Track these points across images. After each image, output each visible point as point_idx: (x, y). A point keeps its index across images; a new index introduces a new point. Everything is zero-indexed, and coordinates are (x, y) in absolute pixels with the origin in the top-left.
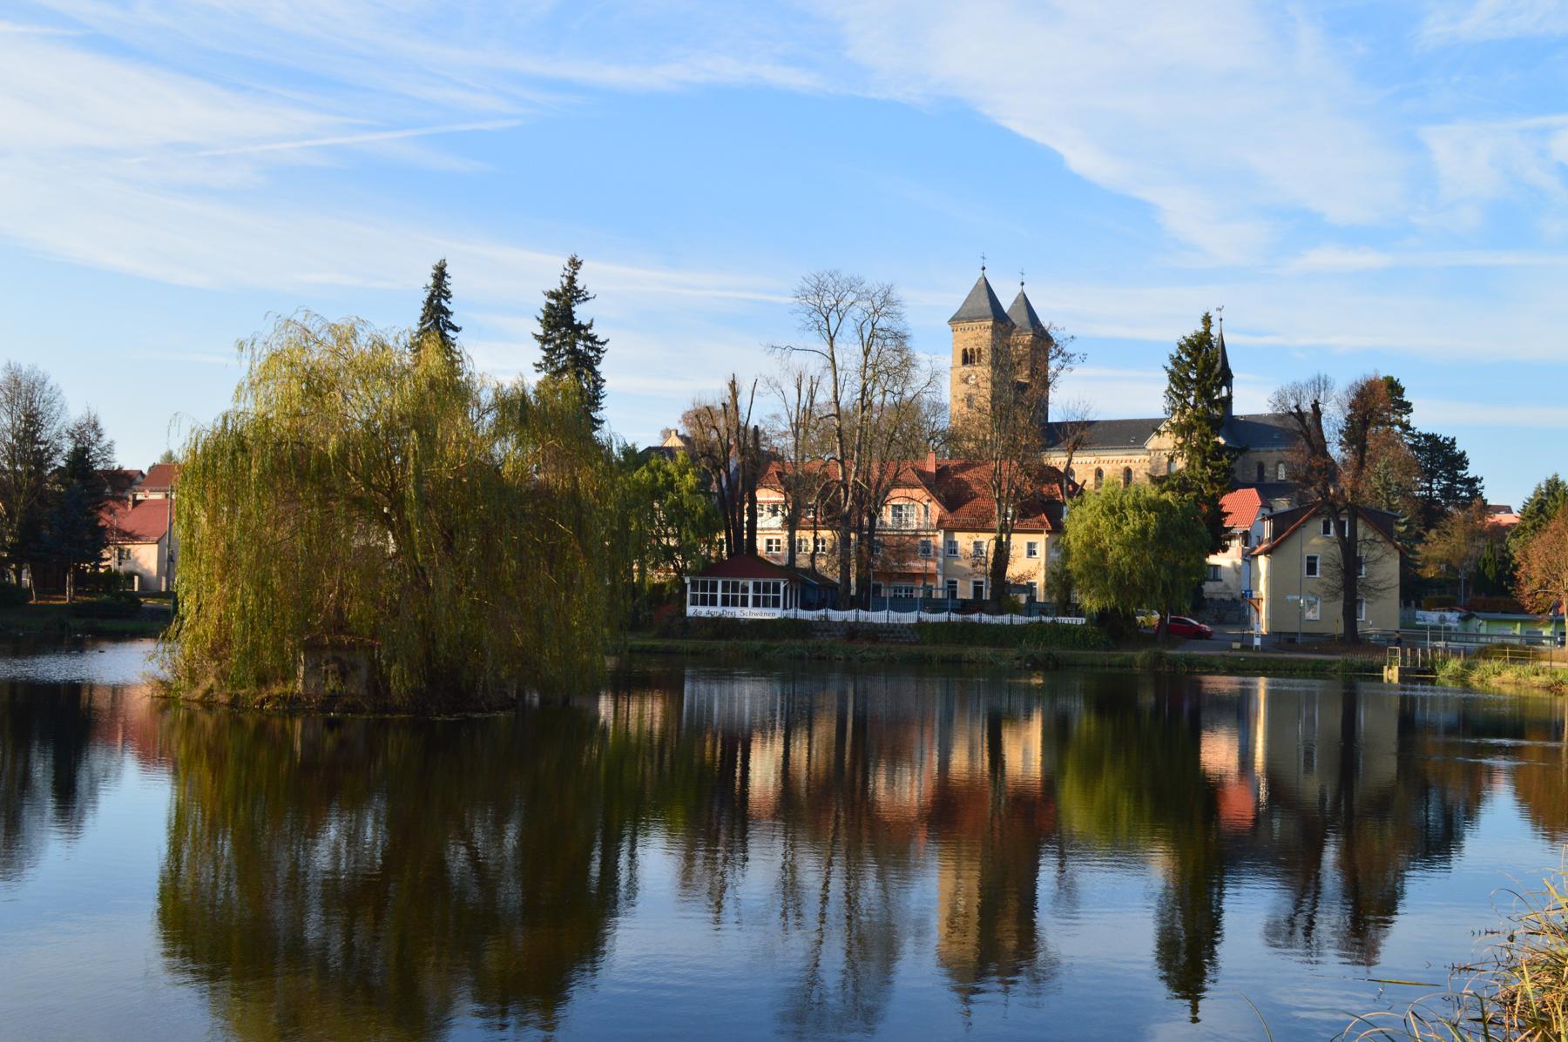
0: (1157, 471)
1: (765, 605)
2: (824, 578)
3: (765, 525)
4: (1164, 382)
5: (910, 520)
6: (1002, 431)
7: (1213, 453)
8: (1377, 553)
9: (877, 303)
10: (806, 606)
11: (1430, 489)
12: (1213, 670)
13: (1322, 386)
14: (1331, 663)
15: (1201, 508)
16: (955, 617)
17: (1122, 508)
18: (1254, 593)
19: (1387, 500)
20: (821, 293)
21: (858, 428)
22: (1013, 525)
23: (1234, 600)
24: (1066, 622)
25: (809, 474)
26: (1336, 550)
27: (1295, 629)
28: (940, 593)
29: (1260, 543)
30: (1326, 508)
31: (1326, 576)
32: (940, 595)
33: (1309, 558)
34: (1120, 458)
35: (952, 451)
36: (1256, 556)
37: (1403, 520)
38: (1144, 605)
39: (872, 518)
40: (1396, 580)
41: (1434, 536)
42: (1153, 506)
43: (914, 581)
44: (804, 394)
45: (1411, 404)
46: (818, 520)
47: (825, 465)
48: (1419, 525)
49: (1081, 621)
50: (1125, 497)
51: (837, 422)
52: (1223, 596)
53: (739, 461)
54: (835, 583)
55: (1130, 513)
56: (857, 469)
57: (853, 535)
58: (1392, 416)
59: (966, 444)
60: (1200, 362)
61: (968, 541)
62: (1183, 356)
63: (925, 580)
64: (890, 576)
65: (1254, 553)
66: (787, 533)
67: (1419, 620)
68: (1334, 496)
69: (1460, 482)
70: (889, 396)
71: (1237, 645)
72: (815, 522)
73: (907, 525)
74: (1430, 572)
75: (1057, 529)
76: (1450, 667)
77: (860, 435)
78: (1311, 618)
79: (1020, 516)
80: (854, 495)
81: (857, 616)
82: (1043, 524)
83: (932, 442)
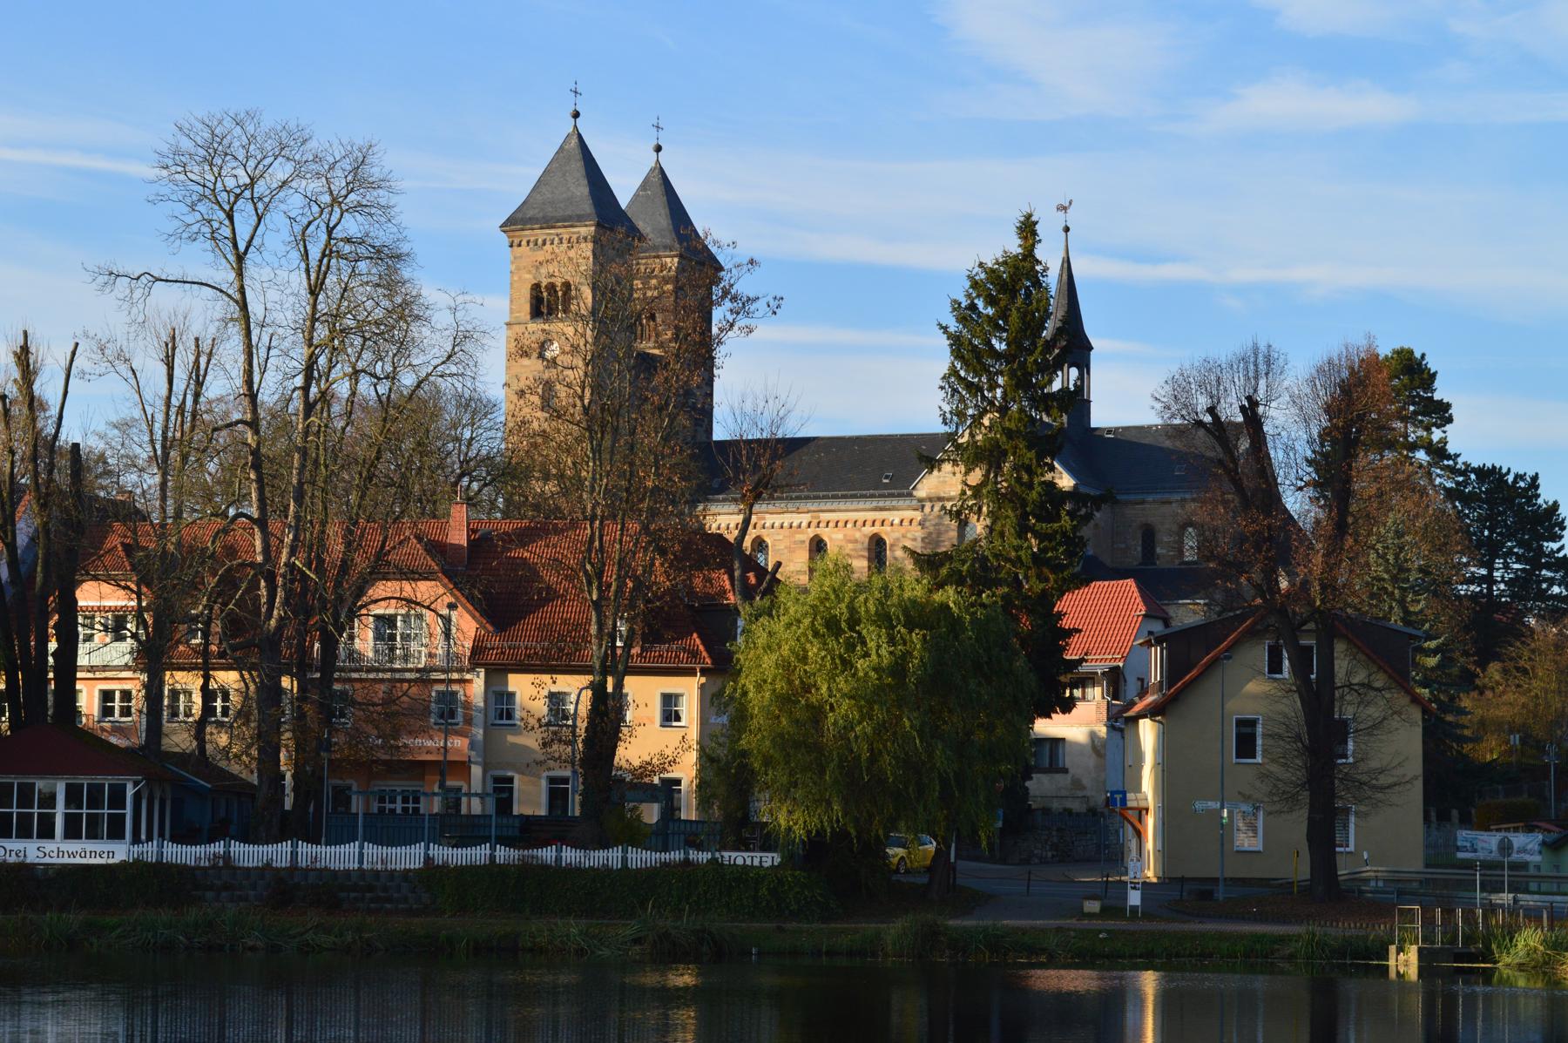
0: (938, 543)
1: (93, 835)
2: (224, 774)
3: (96, 660)
4: (941, 359)
5: (414, 646)
6: (606, 456)
7: (1042, 506)
8: (1374, 712)
9: (339, 184)
10: (183, 836)
11: (1490, 580)
12: (1043, 959)
13: (1263, 368)
14: (1283, 940)
15: (1017, 620)
16: (503, 854)
17: (854, 622)
18: (1130, 796)
19: (1402, 602)
20: (218, 161)
21: (298, 449)
22: (629, 656)
23: (1093, 812)
24: (740, 861)
25: (191, 549)
26: (1292, 706)
27: (1217, 874)
28: (476, 802)
29: (1143, 693)
30: (1272, 620)
31: (1273, 761)
32: (476, 807)
33: (1240, 723)
34: (861, 516)
35: (508, 501)
36: (1134, 720)
37: (1432, 644)
38: (902, 824)
39: (330, 645)
40: (1415, 767)
41: (1497, 677)
42: (918, 616)
43: (422, 778)
44: (181, 374)
45: (1448, 406)
46: (214, 648)
47: (226, 531)
48: (1466, 654)
49: (770, 859)
50: (862, 598)
51: (250, 438)
52: (1069, 804)
53: (38, 521)
54: (251, 785)
55: (873, 636)
56: (296, 538)
57: (286, 682)
58: (1410, 429)
59: (537, 486)
60: (1014, 316)
61: (533, 691)
62: (980, 304)
63: (442, 774)
64: (368, 768)
65: (1131, 713)
66: (144, 677)
67: (1464, 849)
68: (1288, 594)
69: (1548, 567)
70: (364, 385)
71: (1093, 906)
72: (204, 652)
73: (406, 658)
74: (1490, 751)
75: (722, 666)
76: (1521, 945)
77: (303, 467)
78: (1246, 847)
79: (645, 639)
80: (289, 594)
81: (294, 854)
82: (694, 654)
83: (466, 480)
